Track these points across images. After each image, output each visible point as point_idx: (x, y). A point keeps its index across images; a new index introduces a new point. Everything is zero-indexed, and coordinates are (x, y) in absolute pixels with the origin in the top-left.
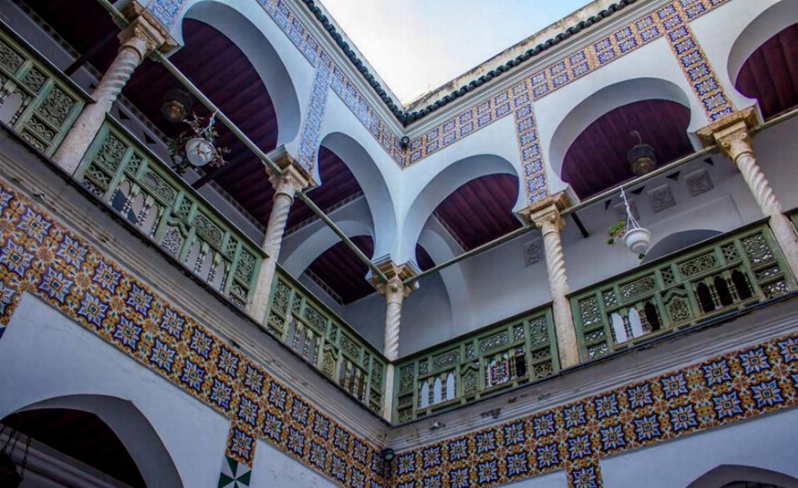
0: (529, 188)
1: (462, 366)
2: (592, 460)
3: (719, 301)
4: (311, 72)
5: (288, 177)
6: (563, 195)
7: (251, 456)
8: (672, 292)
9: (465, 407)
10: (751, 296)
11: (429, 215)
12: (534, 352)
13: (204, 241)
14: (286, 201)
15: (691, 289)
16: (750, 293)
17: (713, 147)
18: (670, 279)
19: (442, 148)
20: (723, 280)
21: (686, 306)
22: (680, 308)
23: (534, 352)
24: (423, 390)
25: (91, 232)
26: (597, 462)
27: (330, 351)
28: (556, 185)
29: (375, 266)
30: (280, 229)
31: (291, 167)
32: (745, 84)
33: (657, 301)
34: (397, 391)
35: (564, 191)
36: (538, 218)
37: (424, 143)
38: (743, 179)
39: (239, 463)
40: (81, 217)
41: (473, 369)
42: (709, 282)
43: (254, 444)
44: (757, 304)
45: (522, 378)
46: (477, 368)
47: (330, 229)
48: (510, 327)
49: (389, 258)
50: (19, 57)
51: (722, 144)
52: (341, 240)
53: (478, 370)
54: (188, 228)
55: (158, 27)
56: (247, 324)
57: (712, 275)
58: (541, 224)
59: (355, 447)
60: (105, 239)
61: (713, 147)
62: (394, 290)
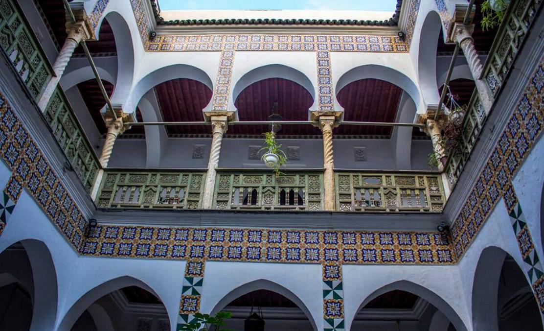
1: (264, 188)
2: (202, 260)
3: (250, 201)
7: (18, 197)
9: (388, 213)
10: (293, 204)
11: (150, 89)
12: (190, 193)
15: (278, 191)
16: (303, 203)
18: (269, 181)
20: (285, 192)
23: (190, 193)
24: (119, 192)
26: (204, 261)
27: (73, 149)
28: (230, 107)
29: (112, 107)
30: (70, 52)
32: (343, 96)
33: (260, 190)
34: (102, 187)
37: (161, 41)
38: (144, 145)
39: (10, 199)
41: (153, 191)
42: (288, 190)
43: (21, 190)
44: (181, 209)
45: (302, 206)
46: (155, 190)
47: (92, 69)
48: (181, 174)
49: (121, 106)
52: (95, 77)
53: (155, 192)
56: (32, 108)
57: (290, 187)
59: (73, 209)
62: (432, 128)
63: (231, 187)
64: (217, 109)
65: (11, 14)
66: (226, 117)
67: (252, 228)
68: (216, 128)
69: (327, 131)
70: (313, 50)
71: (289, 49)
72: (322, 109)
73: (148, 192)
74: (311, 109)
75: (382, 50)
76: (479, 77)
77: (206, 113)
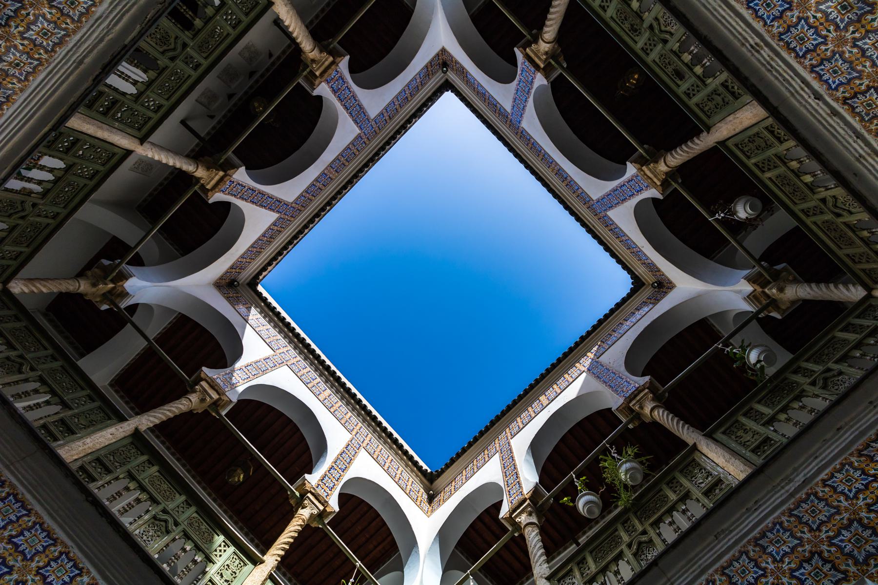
0: (342, 79)
4: (524, 124)
5: (545, 57)
6: (314, 85)
8: (179, 50)
13: (636, 12)
14: (547, 37)
17: (219, 163)
19: (416, 75)
21: (156, 44)
22: (160, 39)
25: (769, 56)
27: (23, 210)
31: (542, 66)
33: (186, 36)
35: (315, 89)
36: (326, 60)
40: (774, 72)
50: (775, 180)
51: (214, 170)
54: (651, 27)
55: (646, 177)
58: (322, 55)
60: (755, 48)
61: (219, 163)
63: (125, 468)
64: (219, 381)
65: (203, 54)
66: (218, 397)
67: (75, 552)
68: (194, 395)
69: (303, 517)
70: (350, 431)
71: (332, 410)
72: (317, 487)
73: (10, 363)
74: (307, 476)
75: (408, 492)
76: (546, 576)
77: (202, 373)
